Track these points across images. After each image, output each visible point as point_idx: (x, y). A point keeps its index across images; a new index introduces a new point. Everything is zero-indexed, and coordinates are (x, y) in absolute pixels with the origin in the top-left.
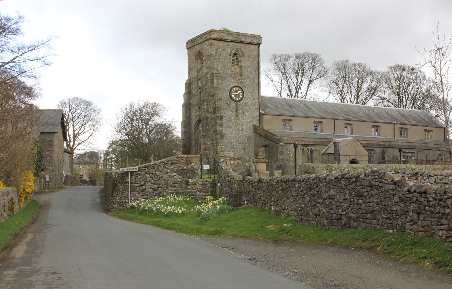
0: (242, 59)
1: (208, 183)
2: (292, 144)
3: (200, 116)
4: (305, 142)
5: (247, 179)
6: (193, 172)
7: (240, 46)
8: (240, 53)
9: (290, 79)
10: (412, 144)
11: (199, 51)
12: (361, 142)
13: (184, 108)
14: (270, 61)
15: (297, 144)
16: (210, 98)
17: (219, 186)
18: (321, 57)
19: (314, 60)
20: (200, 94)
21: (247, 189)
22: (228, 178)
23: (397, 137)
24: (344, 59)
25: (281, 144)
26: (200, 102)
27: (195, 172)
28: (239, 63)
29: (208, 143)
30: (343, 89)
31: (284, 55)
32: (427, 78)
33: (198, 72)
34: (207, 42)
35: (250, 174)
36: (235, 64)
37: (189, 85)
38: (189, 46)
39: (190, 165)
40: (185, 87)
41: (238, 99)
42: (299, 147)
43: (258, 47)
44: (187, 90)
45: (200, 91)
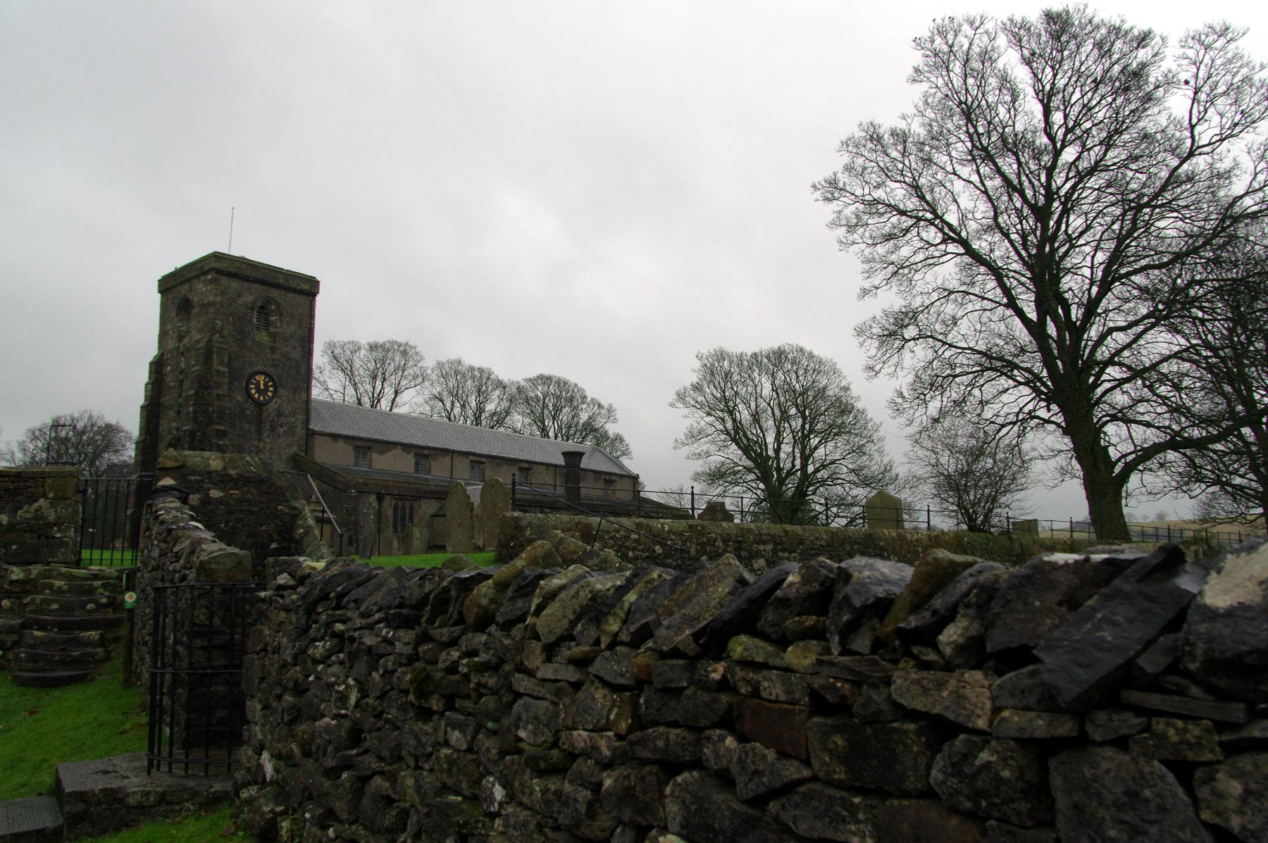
1: (97, 583)
3: (178, 429)
5: (283, 579)
6: (39, 537)
7: (274, 293)
17: (128, 606)
19: (404, 353)
21: (284, 665)
22: (178, 566)
24: (453, 357)
27: (47, 538)
30: (452, 409)
31: (349, 343)
33: (180, 338)
34: (202, 278)
35: (293, 545)
37: (157, 367)
42: (388, 501)
45: (181, 378)
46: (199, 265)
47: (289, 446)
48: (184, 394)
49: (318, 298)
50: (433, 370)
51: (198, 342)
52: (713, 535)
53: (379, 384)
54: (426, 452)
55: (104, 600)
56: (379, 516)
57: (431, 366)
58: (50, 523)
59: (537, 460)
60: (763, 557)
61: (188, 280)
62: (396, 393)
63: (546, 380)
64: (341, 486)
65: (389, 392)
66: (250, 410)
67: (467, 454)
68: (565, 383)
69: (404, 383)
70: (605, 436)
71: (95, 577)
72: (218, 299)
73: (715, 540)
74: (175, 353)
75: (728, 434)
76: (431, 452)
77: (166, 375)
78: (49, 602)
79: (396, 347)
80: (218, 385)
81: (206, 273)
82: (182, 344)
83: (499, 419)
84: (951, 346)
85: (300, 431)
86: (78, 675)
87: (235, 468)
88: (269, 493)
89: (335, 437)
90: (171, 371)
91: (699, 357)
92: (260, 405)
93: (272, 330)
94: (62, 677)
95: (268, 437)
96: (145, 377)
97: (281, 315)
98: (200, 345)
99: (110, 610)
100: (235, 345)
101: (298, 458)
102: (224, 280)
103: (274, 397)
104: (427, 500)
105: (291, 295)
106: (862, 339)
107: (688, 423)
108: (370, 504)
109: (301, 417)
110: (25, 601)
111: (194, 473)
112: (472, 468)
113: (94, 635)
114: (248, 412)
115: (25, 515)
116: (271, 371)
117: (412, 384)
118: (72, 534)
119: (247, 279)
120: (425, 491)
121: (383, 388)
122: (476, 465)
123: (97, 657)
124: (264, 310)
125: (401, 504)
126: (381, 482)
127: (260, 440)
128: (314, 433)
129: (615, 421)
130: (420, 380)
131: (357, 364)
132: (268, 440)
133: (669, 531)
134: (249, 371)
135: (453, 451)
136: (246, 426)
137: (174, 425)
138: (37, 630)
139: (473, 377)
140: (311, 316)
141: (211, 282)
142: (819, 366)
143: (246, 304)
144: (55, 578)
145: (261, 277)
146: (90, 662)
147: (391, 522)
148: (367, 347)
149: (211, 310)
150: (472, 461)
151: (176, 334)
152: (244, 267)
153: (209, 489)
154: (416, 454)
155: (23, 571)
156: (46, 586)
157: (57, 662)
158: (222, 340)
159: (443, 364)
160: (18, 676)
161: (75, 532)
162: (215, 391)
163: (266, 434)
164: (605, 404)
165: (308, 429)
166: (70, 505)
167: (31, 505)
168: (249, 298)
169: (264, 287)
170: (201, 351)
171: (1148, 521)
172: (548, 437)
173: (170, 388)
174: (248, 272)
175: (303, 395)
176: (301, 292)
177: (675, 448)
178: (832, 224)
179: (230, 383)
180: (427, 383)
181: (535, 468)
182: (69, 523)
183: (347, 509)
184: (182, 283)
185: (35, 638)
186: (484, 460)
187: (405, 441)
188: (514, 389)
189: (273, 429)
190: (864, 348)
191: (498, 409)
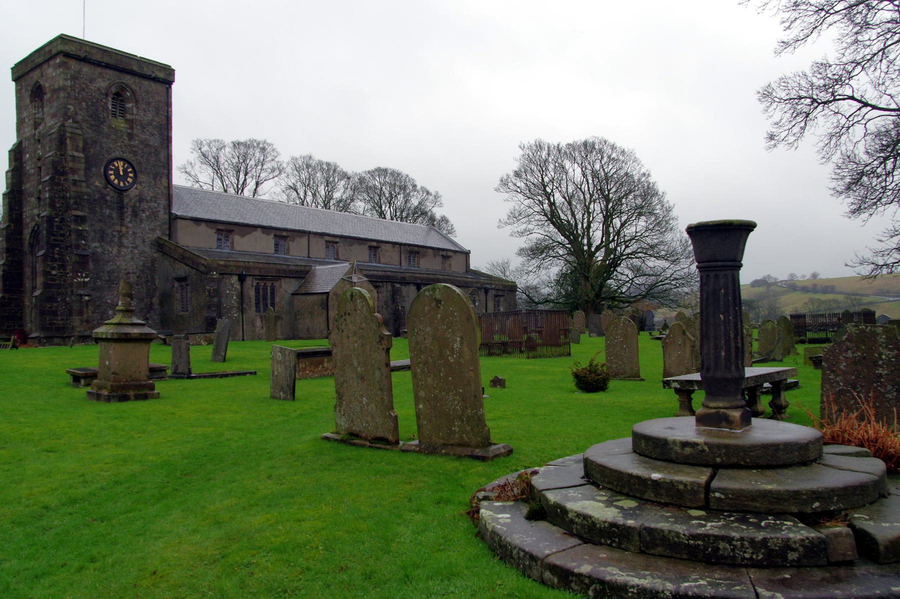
0: (132, 107)
2: (233, 274)
3: (38, 215)
4: (260, 272)
7: (128, 80)
8: (128, 94)
9: (226, 178)
10: (435, 277)
11: (37, 82)
12: (365, 272)
13: (7, 200)
14: (192, 152)
15: (246, 276)
16: (57, 177)
18: (274, 147)
19: (263, 150)
20: (41, 172)
23: (405, 265)
24: (305, 153)
25: (213, 275)
28: (126, 113)
29: (54, 272)
30: (305, 197)
31: (215, 141)
32: (419, 188)
33: (36, 125)
34: (51, 63)
36: (118, 114)
37: (17, 154)
38: (17, 75)
40: (10, 159)
41: (124, 184)
42: (249, 281)
43: (167, 89)
44: (13, 163)
45: (39, 165)
46: (47, 49)
47: (153, 230)
49: (174, 87)
50: (288, 164)
51: (51, 128)
53: (242, 176)
54: (285, 234)
56: (241, 296)
57: (286, 161)
59: (384, 239)
61: (39, 66)
62: (257, 184)
63: (382, 172)
64: (202, 268)
65: (251, 184)
66: (111, 195)
67: (322, 235)
68: (399, 174)
69: (263, 175)
70: (432, 219)
72: (69, 83)
74: (32, 141)
75: (546, 215)
76: (289, 234)
77: (25, 162)
79: (255, 144)
80: (74, 171)
83: (344, 205)
84: (874, 107)
85: (163, 216)
89: (197, 221)
91: (522, 147)
92: (120, 191)
93: (128, 116)
95: (130, 222)
97: (137, 102)
98: (54, 131)
100: (90, 131)
101: (161, 242)
102: (73, 64)
103: (134, 182)
104: (287, 280)
105: (146, 83)
107: (509, 206)
108: (232, 285)
109: (163, 202)
112: (327, 247)
114: (108, 198)
116: (128, 156)
117: (271, 176)
119: (98, 64)
120: (284, 271)
121: (245, 180)
122: (330, 245)
124: (119, 97)
125: (262, 284)
126: (242, 264)
127: (122, 225)
128: (177, 217)
129: (441, 205)
130: (277, 173)
131: (222, 160)
132: (130, 225)
135: (310, 233)
136: (108, 212)
137: (36, 211)
139: (322, 169)
140: (168, 104)
141: (60, 66)
142: (620, 156)
143: (99, 89)
145: (113, 62)
147: (253, 301)
148: (231, 145)
149: (62, 94)
150: (327, 242)
151: (32, 122)
152: (94, 51)
154: (275, 236)
158: (75, 125)
162: (71, 177)
163: (128, 220)
164: (432, 191)
165: (170, 214)
168: (102, 84)
169: (117, 73)
170: (54, 136)
171: (806, 279)
172: (385, 218)
175: (164, 181)
176: (155, 80)
177: (499, 227)
179: (88, 169)
180: (283, 175)
181: (383, 246)
183: (209, 291)
184: (32, 70)
186: (337, 240)
187: (264, 224)
188: (356, 179)
189: (135, 214)
190: (767, 114)
191: (344, 197)
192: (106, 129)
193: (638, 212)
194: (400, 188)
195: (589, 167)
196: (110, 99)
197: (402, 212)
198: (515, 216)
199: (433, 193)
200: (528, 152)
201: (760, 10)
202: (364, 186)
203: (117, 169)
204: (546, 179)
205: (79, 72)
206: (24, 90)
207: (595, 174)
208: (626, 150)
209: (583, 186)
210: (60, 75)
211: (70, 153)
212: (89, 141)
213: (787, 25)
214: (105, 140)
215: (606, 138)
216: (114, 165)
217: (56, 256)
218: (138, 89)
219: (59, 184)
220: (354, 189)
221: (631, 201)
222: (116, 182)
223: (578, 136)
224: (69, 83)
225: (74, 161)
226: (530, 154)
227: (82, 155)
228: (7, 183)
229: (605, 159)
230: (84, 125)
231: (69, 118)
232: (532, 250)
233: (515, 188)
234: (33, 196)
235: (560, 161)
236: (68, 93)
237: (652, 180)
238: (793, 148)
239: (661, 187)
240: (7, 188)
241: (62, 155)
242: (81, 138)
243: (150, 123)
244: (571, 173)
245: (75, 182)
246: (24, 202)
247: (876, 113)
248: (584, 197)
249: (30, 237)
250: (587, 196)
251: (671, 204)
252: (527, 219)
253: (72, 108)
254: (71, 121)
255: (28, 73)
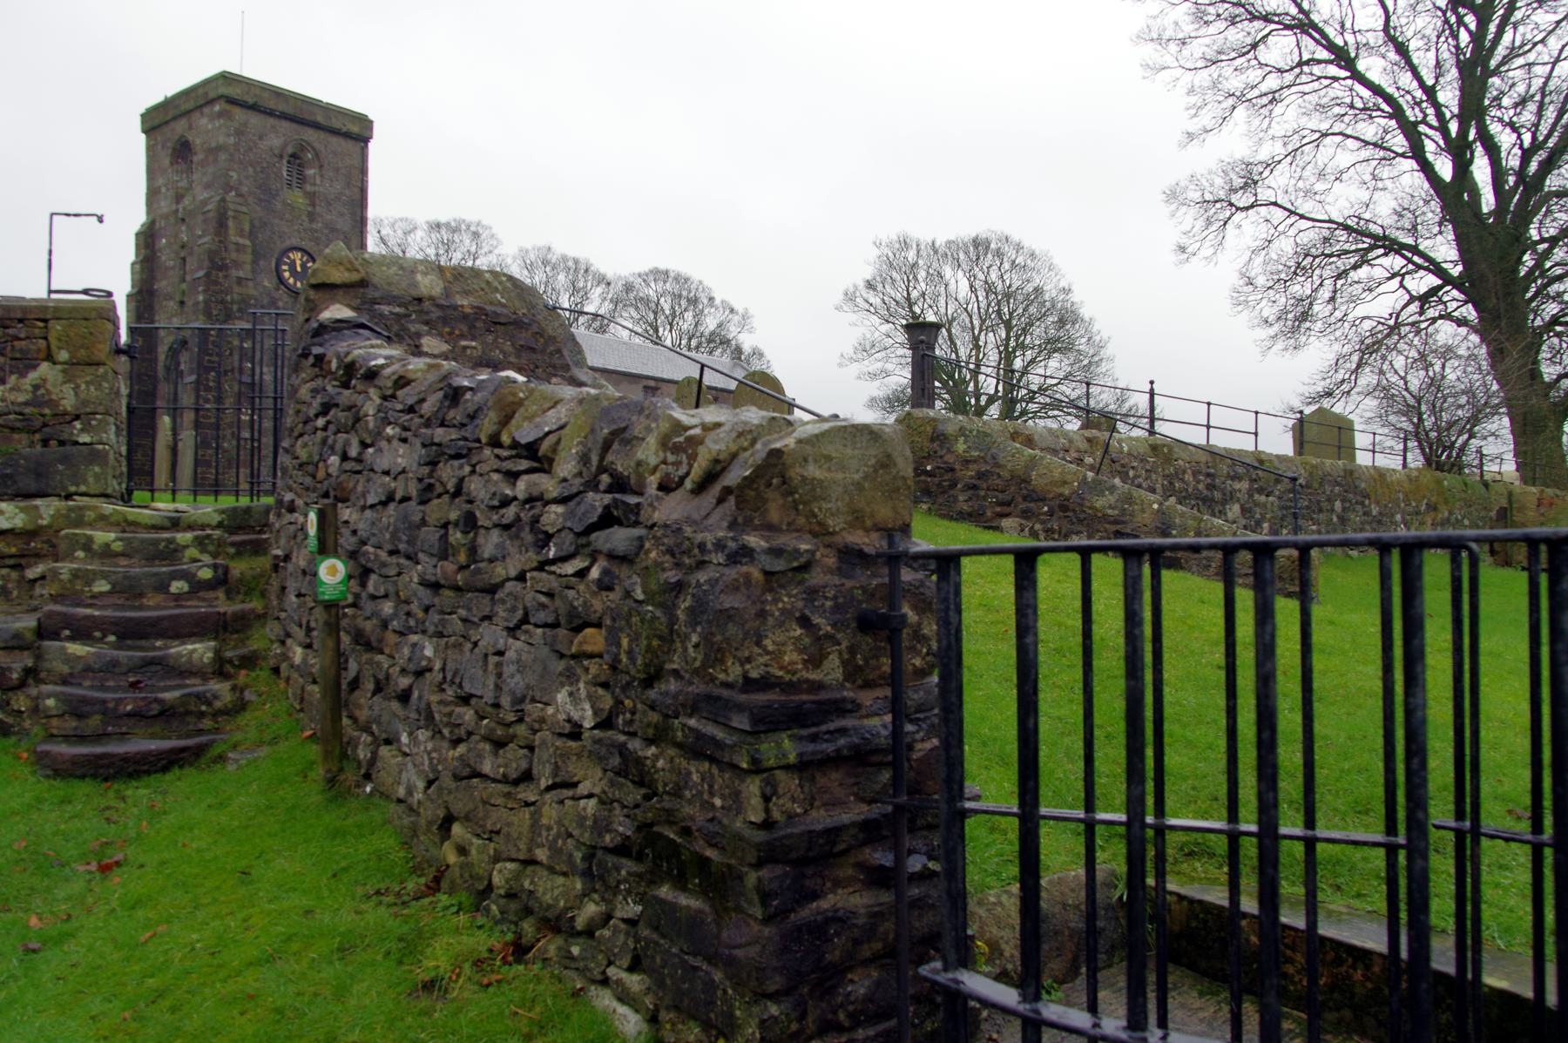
1: (184, 537)
6: (45, 443)
7: (310, 135)
11: (183, 136)
17: (327, 595)
19: (476, 235)
24: (541, 242)
26: (184, 286)
27: (62, 443)
31: (401, 220)
32: (718, 302)
33: (179, 198)
34: (206, 110)
36: (295, 184)
37: (147, 239)
39: (13, 379)
40: (137, 246)
45: (182, 255)
46: (201, 91)
48: (188, 278)
49: (372, 145)
51: (205, 202)
52: (1181, 462)
55: (206, 574)
58: (65, 413)
60: (1238, 501)
61: (188, 113)
63: (661, 275)
68: (686, 280)
70: (738, 351)
71: (175, 523)
72: (232, 140)
73: (1184, 472)
74: (172, 220)
77: (160, 250)
78: (88, 578)
81: (211, 102)
82: (181, 207)
84: (1302, 217)
86: (183, 749)
87: (467, 293)
88: (533, 350)
90: (169, 244)
91: (878, 245)
93: (308, 188)
94: (150, 753)
96: (130, 254)
97: (321, 167)
98: (209, 207)
99: (221, 594)
100: (258, 209)
102: (239, 114)
106: (1173, 207)
110: (31, 574)
111: (391, 299)
113: (199, 650)
115: (11, 397)
118: (113, 436)
119: (270, 113)
123: (218, 704)
124: (296, 159)
133: (1129, 454)
134: (281, 246)
138: (72, 639)
140: (363, 171)
141: (220, 115)
142: (1026, 262)
144: (91, 525)
145: (290, 110)
146: (202, 715)
149: (223, 157)
151: (171, 193)
153: (419, 335)
155: (22, 510)
156: (74, 543)
157: (129, 715)
158: (239, 200)
159: (527, 252)
160: (47, 754)
161: (118, 435)
162: (234, 273)
166: (104, 377)
167: (23, 375)
168: (275, 142)
173: (167, 269)
174: (271, 104)
176: (347, 135)
177: (840, 365)
178: (1138, 37)
179: (255, 262)
181: (663, 386)
182: (107, 413)
184: (175, 118)
185: (71, 659)
192: (279, 206)
193: (1053, 346)
194: (688, 300)
195: (981, 276)
196: (285, 162)
197: (690, 339)
198: (866, 349)
199: (741, 311)
200: (887, 251)
201: (1170, 86)
202: (632, 296)
203: (292, 265)
204: (915, 294)
205: (245, 124)
206: (159, 147)
207: (989, 288)
208: (1037, 252)
209: (970, 307)
210: (220, 128)
211: (233, 238)
212: (257, 223)
213: (1193, 111)
214: (276, 221)
215: (1007, 232)
216: (289, 258)
217: (211, 384)
218: (323, 149)
219: (216, 283)
220: (616, 302)
221: (1037, 334)
222: (291, 281)
223: (966, 230)
224: (232, 140)
225: (238, 251)
226: (890, 255)
227: (248, 243)
228: (133, 280)
229: (1007, 266)
230: (251, 200)
231: (231, 189)
232: (888, 400)
233: (867, 306)
234: (171, 298)
235: (935, 265)
236: (231, 155)
237: (1076, 297)
238: (1212, 264)
239: (1086, 312)
240: (133, 287)
241: (220, 242)
242: (248, 217)
243: (338, 198)
244: (952, 287)
245: (240, 281)
246: (157, 307)
247: (1304, 224)
248: (972, 322)
249: (167, 356)
250: (976, 323)
251: (1105, 337)
252: (883, 354)
253: (234, 175)
254: (233, 193)
255: (167, 123)
